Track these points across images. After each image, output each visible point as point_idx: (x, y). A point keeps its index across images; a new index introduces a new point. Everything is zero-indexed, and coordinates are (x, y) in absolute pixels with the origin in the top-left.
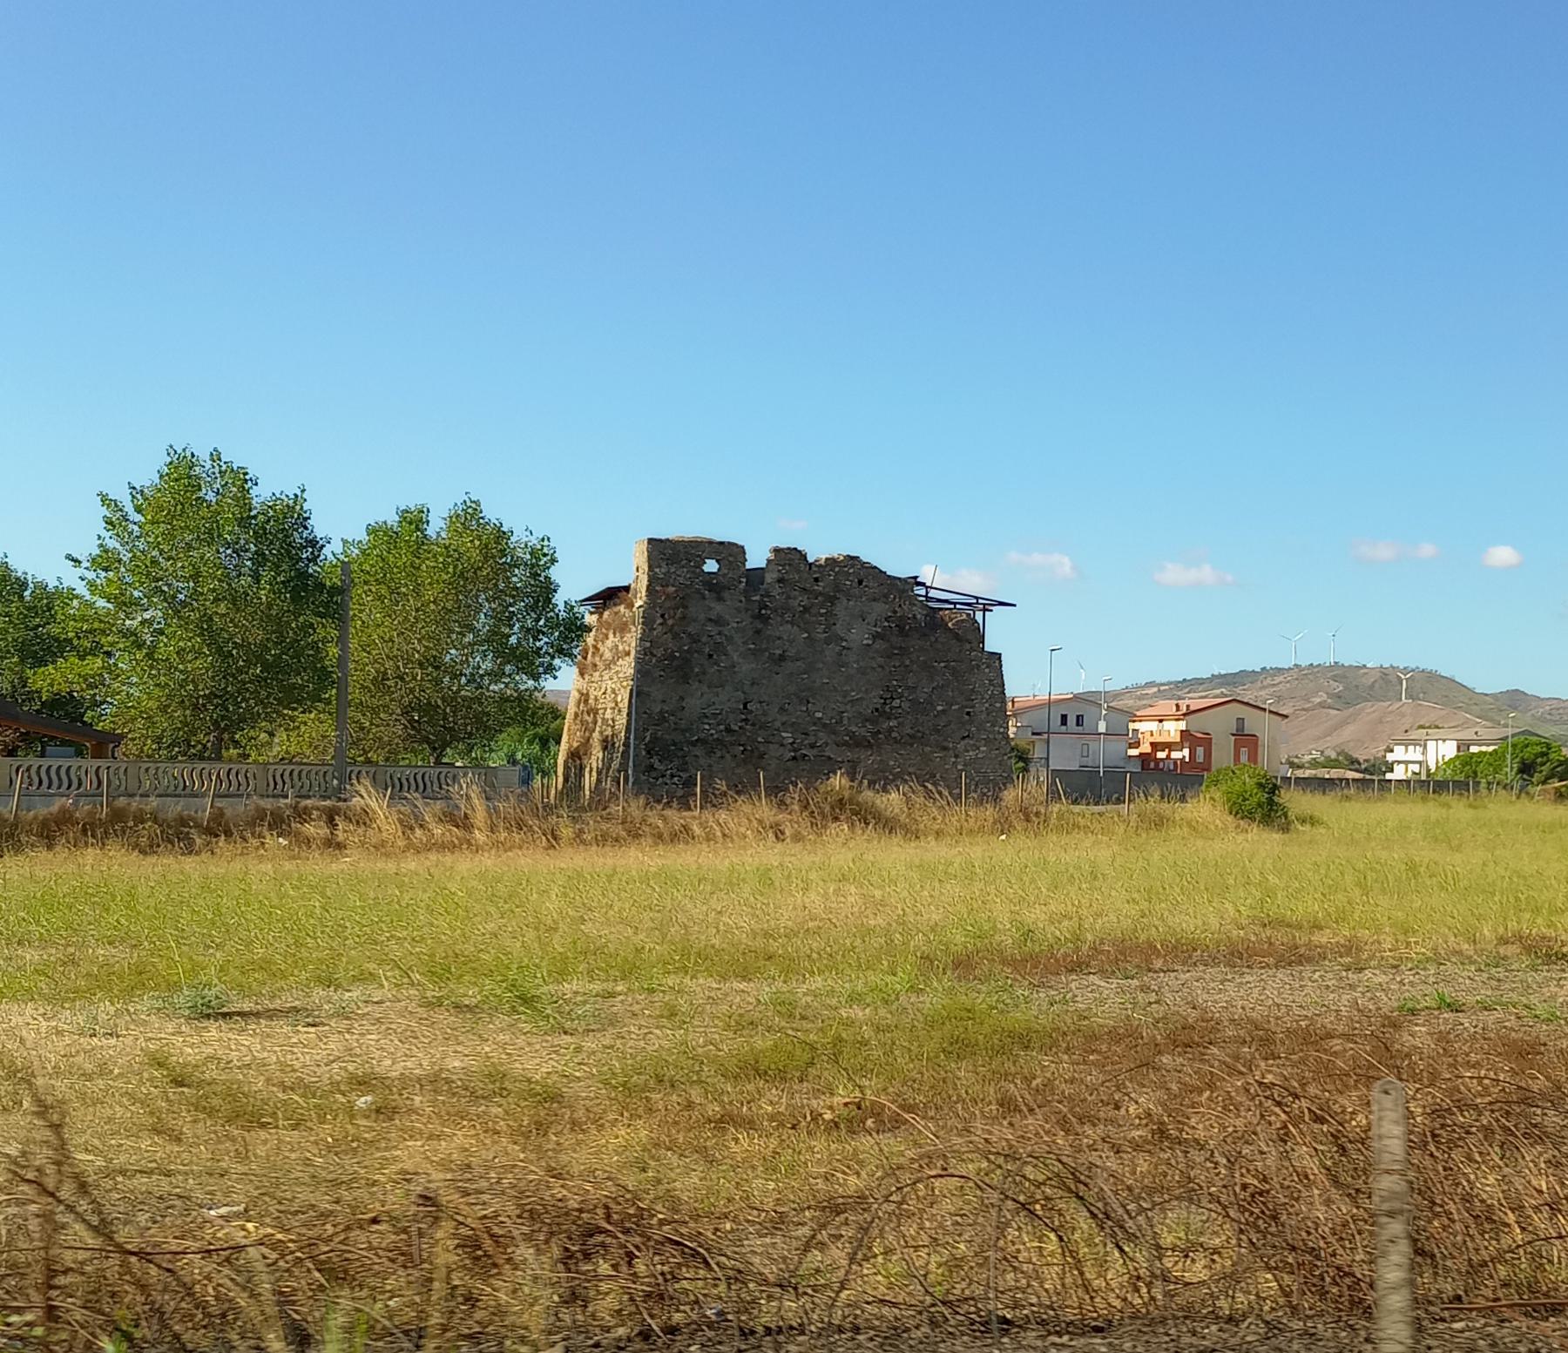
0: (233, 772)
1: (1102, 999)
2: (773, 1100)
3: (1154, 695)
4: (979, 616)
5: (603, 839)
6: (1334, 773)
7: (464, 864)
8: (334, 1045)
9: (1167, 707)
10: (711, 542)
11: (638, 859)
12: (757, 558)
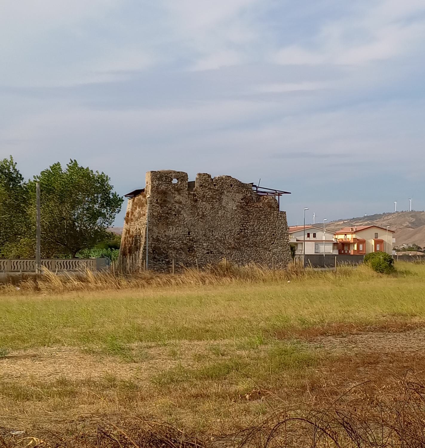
0: (18, 263)
1: (336, 347)
2: (215, 388)
3: (342, 225)
4: (277, 197)
5: (137, 286)
6: (411, 254)
7: (89, 296)
8: (50, 369)
9: (348, 229)
10: (174, 172)
11: (150, 293)
12: (192, 177)
